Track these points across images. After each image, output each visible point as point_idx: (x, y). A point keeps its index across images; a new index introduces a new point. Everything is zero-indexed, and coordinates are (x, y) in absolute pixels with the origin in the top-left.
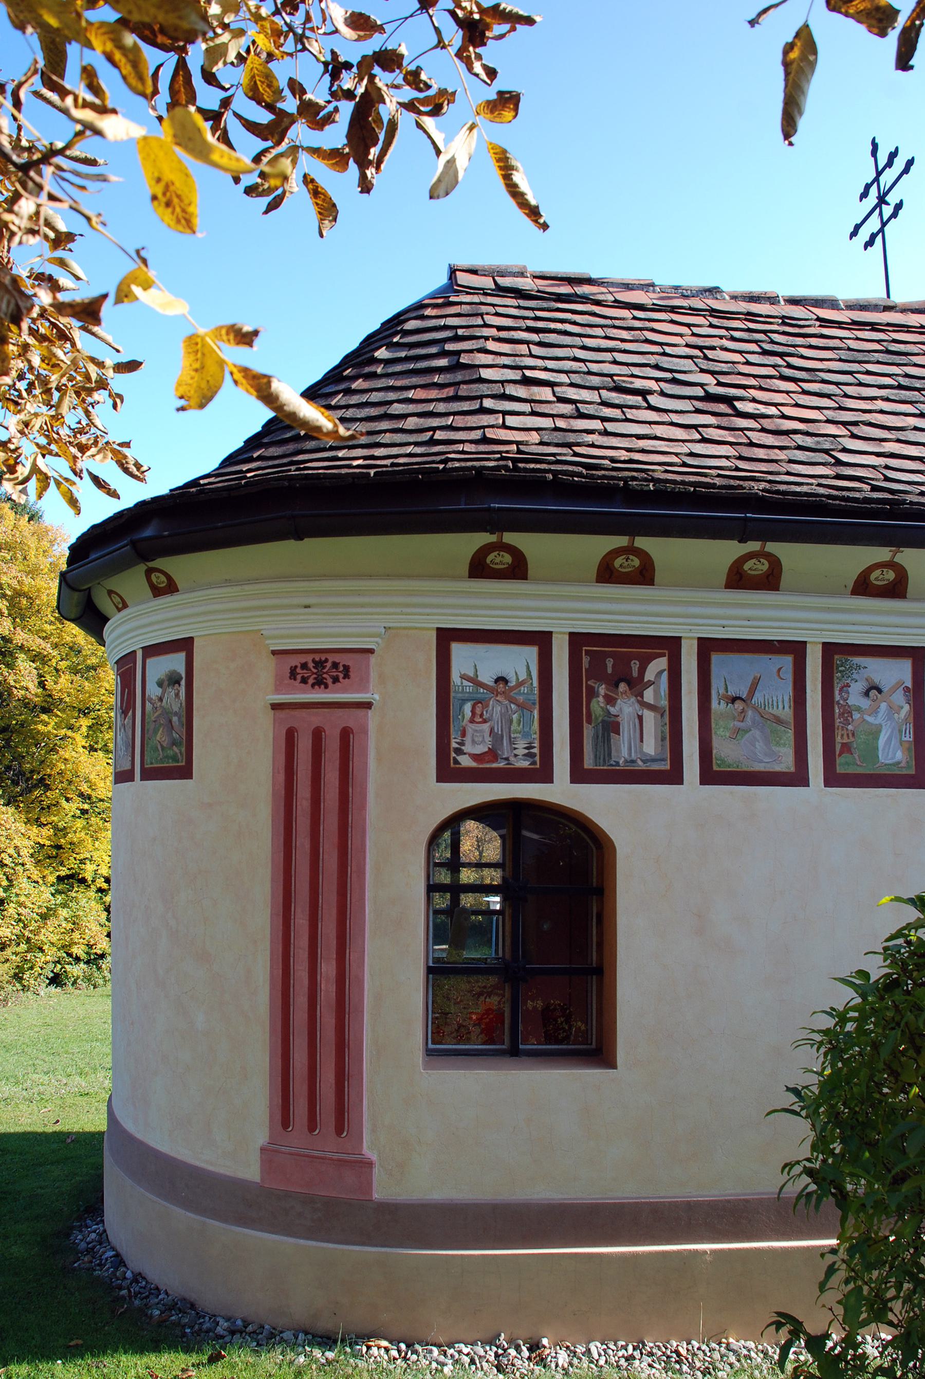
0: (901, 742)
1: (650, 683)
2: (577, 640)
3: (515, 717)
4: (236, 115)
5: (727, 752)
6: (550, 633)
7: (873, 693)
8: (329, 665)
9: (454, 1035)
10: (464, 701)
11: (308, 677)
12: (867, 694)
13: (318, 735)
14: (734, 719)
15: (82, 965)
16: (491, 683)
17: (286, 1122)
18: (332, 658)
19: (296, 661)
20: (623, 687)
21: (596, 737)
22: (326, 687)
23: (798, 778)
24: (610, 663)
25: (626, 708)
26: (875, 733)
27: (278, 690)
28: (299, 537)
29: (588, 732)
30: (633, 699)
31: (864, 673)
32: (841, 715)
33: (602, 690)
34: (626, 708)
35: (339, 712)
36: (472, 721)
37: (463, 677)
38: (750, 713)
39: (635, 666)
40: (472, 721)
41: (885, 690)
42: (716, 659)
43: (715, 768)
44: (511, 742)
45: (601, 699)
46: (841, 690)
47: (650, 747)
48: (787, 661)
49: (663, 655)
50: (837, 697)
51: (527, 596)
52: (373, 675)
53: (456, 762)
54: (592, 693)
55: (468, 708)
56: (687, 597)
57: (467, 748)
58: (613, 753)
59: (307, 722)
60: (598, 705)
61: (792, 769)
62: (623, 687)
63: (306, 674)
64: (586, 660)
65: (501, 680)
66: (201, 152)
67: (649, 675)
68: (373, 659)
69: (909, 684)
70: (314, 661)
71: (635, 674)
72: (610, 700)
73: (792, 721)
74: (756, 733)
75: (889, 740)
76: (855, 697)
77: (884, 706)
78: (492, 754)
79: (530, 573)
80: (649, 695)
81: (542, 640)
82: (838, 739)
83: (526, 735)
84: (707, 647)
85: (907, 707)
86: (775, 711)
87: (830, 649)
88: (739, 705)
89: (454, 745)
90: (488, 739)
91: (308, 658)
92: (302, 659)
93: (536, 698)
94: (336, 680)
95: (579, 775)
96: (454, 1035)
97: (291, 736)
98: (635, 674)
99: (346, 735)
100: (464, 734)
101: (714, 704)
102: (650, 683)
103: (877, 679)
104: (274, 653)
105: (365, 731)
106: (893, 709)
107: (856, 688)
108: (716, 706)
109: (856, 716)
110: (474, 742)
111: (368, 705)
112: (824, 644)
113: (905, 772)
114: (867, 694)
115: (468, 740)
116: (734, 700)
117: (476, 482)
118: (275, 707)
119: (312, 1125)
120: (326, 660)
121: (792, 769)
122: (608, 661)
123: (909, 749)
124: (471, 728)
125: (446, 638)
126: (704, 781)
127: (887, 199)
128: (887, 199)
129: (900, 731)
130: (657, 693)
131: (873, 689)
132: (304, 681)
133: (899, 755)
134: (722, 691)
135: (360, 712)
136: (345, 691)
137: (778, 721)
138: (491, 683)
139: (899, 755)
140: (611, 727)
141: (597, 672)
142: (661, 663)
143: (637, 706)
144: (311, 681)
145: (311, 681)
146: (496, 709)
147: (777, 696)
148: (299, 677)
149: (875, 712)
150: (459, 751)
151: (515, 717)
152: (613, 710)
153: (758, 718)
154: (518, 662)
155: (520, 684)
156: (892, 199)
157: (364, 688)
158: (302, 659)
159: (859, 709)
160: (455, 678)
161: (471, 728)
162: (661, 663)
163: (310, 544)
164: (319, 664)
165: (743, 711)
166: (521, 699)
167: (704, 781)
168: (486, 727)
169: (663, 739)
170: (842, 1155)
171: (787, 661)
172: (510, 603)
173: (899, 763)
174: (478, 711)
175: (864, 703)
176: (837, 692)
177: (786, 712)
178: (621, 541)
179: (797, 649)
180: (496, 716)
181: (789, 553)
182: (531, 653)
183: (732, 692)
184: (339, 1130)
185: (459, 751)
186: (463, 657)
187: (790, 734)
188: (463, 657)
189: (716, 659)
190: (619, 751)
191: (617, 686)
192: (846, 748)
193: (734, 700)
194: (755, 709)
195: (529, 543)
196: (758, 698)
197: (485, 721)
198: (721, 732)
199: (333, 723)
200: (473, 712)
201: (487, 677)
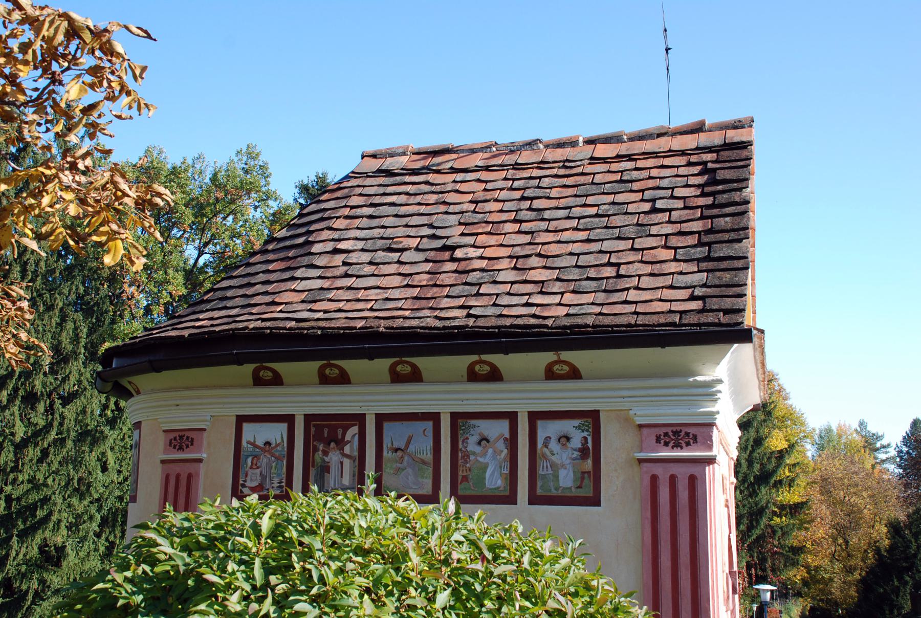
0: (501, 474)
1: (348, 442)
2: (308, 418)
3: (274, 465)
6: (294, 415)
7: (484, 442)
10: (248, 457)
11: (669, 442)
12: (479, 443)
13: (673, 478)
14: (397, 462)
16: (262, 445)
18: (685, 430)
19: (661, 431)
20: (333, 445)
21: (316, 475)
22: (682, 448)
24: (326, 431)
25: (334, 457)
26: (485, 468)
27: (165, 453)
28: (158, 370)
29: (312, 472)
30: (338, 452)
31: (478, 430)
32: (463, 457)
33: (321, 447)
35: (188, 464)
36: (251, 468)
37: (248, 443)
38: (406, 458)
39: (340, 431)
40: (251, 468)
41: (491, 440)
42: (386, 425)
44: (271, 480)
45: (320, 453)
46: (463, 441)
48: (429, 425)
49: (355, 425)
50: (460, 446)
51: (489, 391)
52: (205, 443)
53: (242, 492)
54: (316, 449)
55: (249, 460)
56: (368, 393)
57: (248, 484)
58: (326, 485)
59: (176, 469)
60: (319, 456)
61: (430, 493)
62: (333, 445)
64: (313, 430)
65: (268, 443)
67: (348, 437)
68: (205, 434)
69: (507, 436)
70: (672, 431)
71: (340, 437)
72: (325, 453)
73: (432, 462)
74: (409, 470)
75: (493, 472)
76: (472, 446)
77: (490, 451)
79: (352, 381)
80: (347, 449)
81: (289, 419)
82: (460, 473)
83: (279, 475)
84: (381, 419)
85: (505, 451)
86: (421, 456)
87: (455, 416)
88: (399, 453)
89: (241, 482)
90: (259, 478)
91: (669, 430)
93: (285, 453)
94: (187, 446)
97: (654, 479)
98: (340, 437)
99: (190, 476)
100: (246, 476)
101: (385, 454)
102: (348, 442)
103: (486, 433)
104: (164, 431)
105: (198, 474)
106: (497, 453)
107: (473, 439)
108: (386, 454)
109: (472, 458)
110: (251, 480)
111: (200, 461)
112: (451, 413)
113: (502, 494)
114: (479, 443)
115: (248, 479)
116: (397, 450)
117: (257, 336)
118: (163, 462)
120: (681, 431)
121: (430, 493)
122: (325, 430)
123: (506, 478)
124: (250, 472)
125: (241, 420)
126: (531, 502)
129: (501, 467)
130: (352, 449)
131: (484, 440)
132: (175, 447)
133: (499, 483)
134: (390, 445)
135: (196, 464)
136: (190, 453)
137: (424, 462)
138: (262, 445)
139: (499, 483)
141: (319, 437)
142: (354, 430)
143: (340, 456)
144: (671, 444)
145: (671, 444)
146: (264, 461)
147: (423, 447)
148: (662, 442)
149: (484, 454)
150: (244, 486)
151: (274, 465)
152: (327, 459)
153: (411, 461)
154: (276, 433)
155: (277, 445)
157: (199, 451)
158: (665, 430)
159: (474, 453)
160: (244, 443)
161: (250, 472)
162: (354, 430)
163: (165, 374)
164: (676, 433)
165: (402, 457)
166: (277, 454)
167: (531, 502)
168: (258, 471)
169: (354, 476)
171: (429, 425)
172: (343, 398)
173: (499, 488)
174: (255, 462)
175: (478, 449)
176: (460, 443)
177: (429, 457)
178: (475, 358)
179: (435, 418)
180: (264, 465)
181: (423, 363)
182: (283, 427)
183: (396, 445)
185: (244, 486)
186: (249, 430)
187: (430, 470)
188: (249, 430)
189: (386, 425)
190: (329, 483)
191: (329, 445)
192: (465, 478)
193: (397, 450)
194: (409, 455)
195: (349, 365)
196: (411, 448)
197: (258, 468)
198: (388, 470)
199: (683, 472)
200: (252, 462)
201: (260, 443)
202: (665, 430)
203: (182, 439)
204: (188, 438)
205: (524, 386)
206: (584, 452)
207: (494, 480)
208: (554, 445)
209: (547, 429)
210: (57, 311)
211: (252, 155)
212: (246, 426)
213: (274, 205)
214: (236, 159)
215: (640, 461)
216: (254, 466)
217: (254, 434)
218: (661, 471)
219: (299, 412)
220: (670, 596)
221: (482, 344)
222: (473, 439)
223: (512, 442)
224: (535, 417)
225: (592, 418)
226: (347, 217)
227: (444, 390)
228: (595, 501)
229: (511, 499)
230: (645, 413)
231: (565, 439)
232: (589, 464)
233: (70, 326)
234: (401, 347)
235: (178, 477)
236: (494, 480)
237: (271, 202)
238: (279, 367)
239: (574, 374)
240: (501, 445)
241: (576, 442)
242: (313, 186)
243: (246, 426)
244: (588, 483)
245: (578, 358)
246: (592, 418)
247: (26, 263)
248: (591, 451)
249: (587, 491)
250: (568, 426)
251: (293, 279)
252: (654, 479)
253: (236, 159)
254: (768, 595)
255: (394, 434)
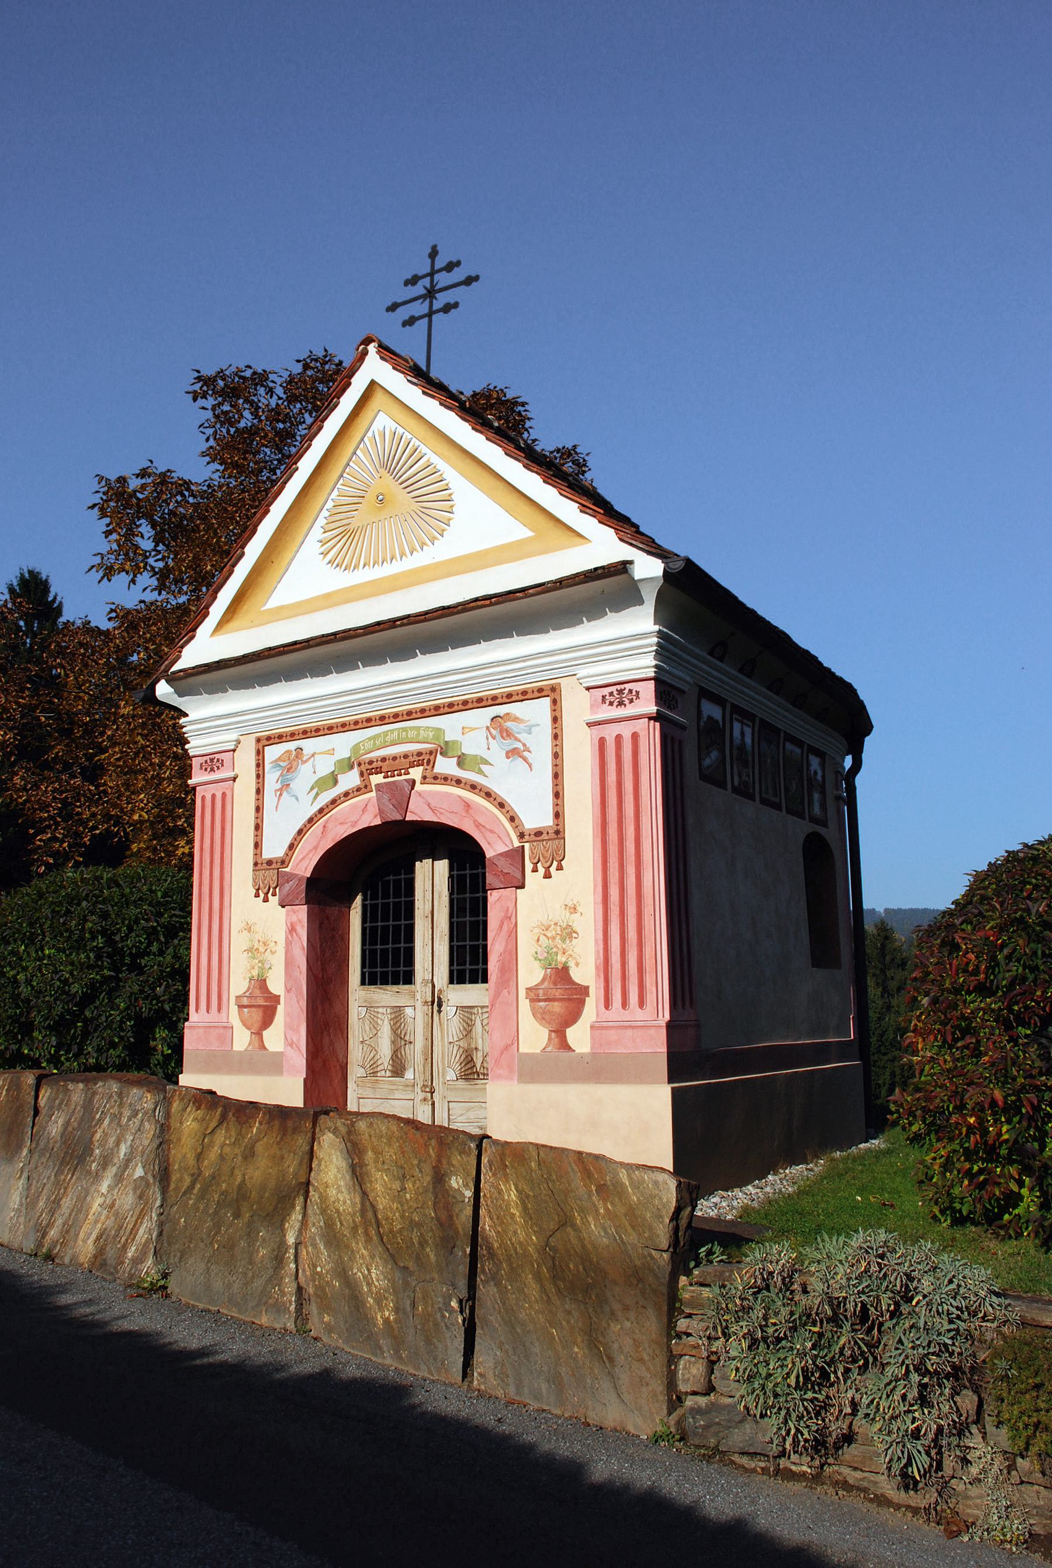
4: (88, 1106)
8: (626, 691)
9: (370, 979)
13: (619, 738)
43: (418, 864)
59: (610, 732)
63: (612, 699)
66: (327, 378)
91: (613, 689)
92: (606, 691)
94: (631, 701)
96: (370, 979)
97: (602, 742)
104: (588, 689)
118: (590, 725)
127: (424, 292)
128: (424, 292)
132: (611, 704)
144: (615, 704)
145: (615, 704)
156: (419, 289)
184: (219, 1009)
202: (205, 758)
204: (631, 691)
220: (633, 858)
235: (214, 796)
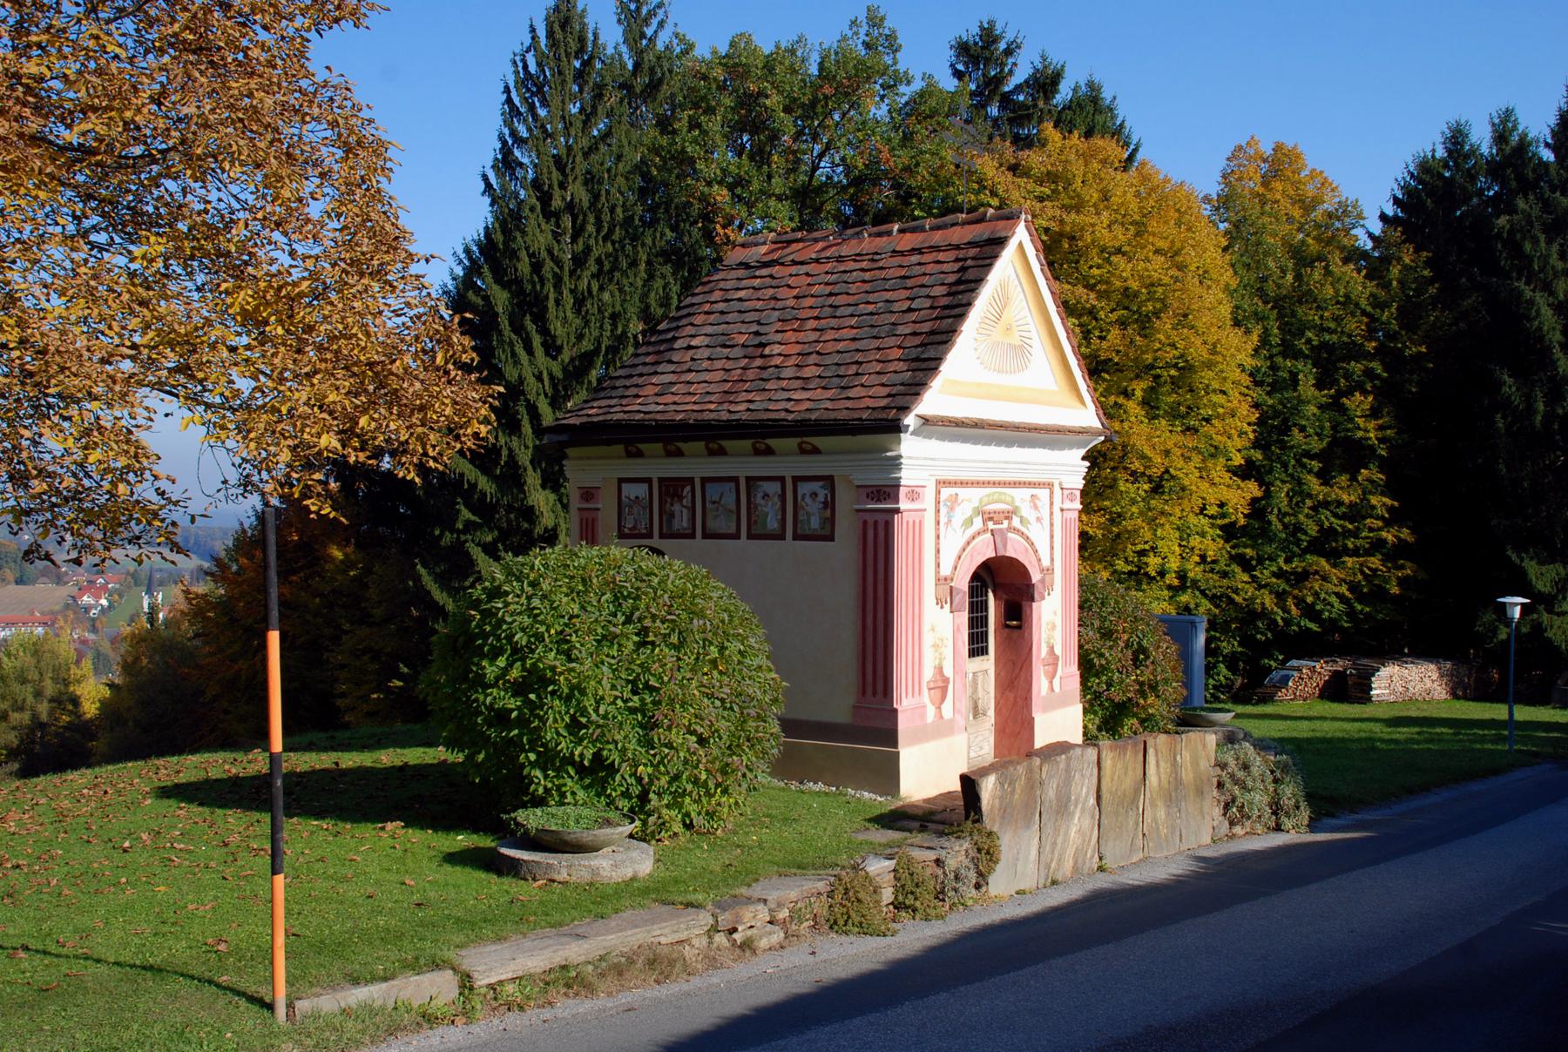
5: (712, 525)
13: (876, 522)
15: (33, 661)
17: (864, 693)
23: (737, 536)
25: (677, 508)
34: (677, 508)
42: (708, 485)
47: (685, 524)
48: (733, 485)
56: (694, 465)
76: (759, 500)
78: (634, 528)
81: (648, 481)
84: (704, 480)
87: (748, 479)
95: (662, 536)
97: (865, 522)
107: (760, 495)
119: (874, 694)
122: (672, 488)
125: (621, 481)
131: (766, 495)
140: (672, 515)
142: (688, 488)
146: (635, 510)
147: (729, 500)
154: (640, 490)
162: (688, 488)
170: (478, 765)
171: (733, 485)
177: (734, 507)
179: (735, 480)
182: (645, 486)
189: (708, 485)
199: (881, 518)
203: (588, 494)
205: (786, 462)
206: (825, 504)
207: (772, 524)
208: (808, 500)
209: (804, 488)
210: (643, 266)
211: (875, 20)
212: (624, 485)
213: (906, 92)
214: (850, 34)
215: (858, 511)
216: (630, 513)
217: (631, 491)
218: (870, 518)
219: (655, 475)
221: (761, 433)
222: (760, 495)
223: (783, 497)
224: (797, 480)
225: (829, 481)
226: (707, 313)
227: (740, 463)
228: (831, 538)
229: (782, 537)
230: (861, 478)
231: (814, 495)
232: (828, 513)
233: (659, 283)
234: (713, 434)
236: (772, 524)
237: (902, 89)
238: (641, 446)
239: (816, 451)
240: (776, 499)
241: (821, 498)
242: (976, 44)
243: (624, 485)
244: (828, 526)
245: (817, 441)
246: (829, 481)
247: (600, 211)
248: (830, 504)
249: (826, 532)
250: (815, 486)
251: (656, 373)
252: (865, 522)
253: (850, 34)
254: (1518, 609)
255: (713, 491)
